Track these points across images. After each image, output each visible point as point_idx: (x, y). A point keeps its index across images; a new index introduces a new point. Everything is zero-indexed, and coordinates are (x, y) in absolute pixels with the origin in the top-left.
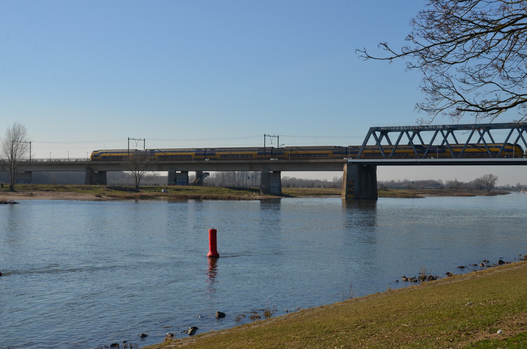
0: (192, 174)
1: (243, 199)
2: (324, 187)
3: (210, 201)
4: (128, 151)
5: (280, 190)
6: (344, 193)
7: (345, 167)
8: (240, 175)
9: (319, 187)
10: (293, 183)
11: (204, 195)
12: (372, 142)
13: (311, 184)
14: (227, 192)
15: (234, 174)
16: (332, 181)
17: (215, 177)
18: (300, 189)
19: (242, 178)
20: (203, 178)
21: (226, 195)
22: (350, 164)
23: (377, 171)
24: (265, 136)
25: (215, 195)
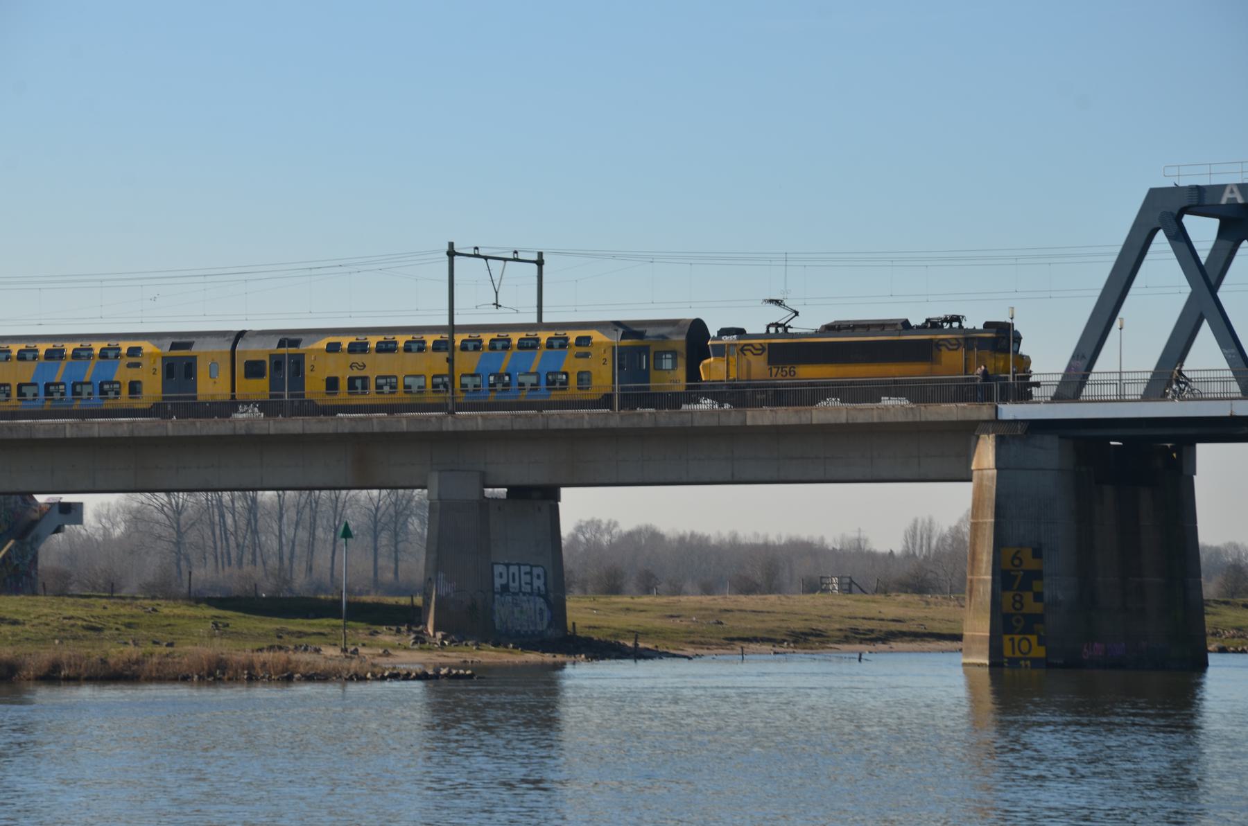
1: (309, 678)
2: (849, 587)
3: (86, 692)
4: (449, 340)
5: (558, 611)
6: (978, 626)
7: (985, 455)
8: (290, 515)
9: (814, 586)
10: (643, 566)
11: (46, 655)
12: (772, 330)
13: (763, 569)
14: (205, 628)
15: (253, 507)
16: (898, 548)
17: (118, 532)
18: (691, 600)
19: (303, 535)
20: (38, 539)
21: (200, 647)
22: (1012, 437)
23: (1197, 479)
24: (452, 253)
25: (118, 652)
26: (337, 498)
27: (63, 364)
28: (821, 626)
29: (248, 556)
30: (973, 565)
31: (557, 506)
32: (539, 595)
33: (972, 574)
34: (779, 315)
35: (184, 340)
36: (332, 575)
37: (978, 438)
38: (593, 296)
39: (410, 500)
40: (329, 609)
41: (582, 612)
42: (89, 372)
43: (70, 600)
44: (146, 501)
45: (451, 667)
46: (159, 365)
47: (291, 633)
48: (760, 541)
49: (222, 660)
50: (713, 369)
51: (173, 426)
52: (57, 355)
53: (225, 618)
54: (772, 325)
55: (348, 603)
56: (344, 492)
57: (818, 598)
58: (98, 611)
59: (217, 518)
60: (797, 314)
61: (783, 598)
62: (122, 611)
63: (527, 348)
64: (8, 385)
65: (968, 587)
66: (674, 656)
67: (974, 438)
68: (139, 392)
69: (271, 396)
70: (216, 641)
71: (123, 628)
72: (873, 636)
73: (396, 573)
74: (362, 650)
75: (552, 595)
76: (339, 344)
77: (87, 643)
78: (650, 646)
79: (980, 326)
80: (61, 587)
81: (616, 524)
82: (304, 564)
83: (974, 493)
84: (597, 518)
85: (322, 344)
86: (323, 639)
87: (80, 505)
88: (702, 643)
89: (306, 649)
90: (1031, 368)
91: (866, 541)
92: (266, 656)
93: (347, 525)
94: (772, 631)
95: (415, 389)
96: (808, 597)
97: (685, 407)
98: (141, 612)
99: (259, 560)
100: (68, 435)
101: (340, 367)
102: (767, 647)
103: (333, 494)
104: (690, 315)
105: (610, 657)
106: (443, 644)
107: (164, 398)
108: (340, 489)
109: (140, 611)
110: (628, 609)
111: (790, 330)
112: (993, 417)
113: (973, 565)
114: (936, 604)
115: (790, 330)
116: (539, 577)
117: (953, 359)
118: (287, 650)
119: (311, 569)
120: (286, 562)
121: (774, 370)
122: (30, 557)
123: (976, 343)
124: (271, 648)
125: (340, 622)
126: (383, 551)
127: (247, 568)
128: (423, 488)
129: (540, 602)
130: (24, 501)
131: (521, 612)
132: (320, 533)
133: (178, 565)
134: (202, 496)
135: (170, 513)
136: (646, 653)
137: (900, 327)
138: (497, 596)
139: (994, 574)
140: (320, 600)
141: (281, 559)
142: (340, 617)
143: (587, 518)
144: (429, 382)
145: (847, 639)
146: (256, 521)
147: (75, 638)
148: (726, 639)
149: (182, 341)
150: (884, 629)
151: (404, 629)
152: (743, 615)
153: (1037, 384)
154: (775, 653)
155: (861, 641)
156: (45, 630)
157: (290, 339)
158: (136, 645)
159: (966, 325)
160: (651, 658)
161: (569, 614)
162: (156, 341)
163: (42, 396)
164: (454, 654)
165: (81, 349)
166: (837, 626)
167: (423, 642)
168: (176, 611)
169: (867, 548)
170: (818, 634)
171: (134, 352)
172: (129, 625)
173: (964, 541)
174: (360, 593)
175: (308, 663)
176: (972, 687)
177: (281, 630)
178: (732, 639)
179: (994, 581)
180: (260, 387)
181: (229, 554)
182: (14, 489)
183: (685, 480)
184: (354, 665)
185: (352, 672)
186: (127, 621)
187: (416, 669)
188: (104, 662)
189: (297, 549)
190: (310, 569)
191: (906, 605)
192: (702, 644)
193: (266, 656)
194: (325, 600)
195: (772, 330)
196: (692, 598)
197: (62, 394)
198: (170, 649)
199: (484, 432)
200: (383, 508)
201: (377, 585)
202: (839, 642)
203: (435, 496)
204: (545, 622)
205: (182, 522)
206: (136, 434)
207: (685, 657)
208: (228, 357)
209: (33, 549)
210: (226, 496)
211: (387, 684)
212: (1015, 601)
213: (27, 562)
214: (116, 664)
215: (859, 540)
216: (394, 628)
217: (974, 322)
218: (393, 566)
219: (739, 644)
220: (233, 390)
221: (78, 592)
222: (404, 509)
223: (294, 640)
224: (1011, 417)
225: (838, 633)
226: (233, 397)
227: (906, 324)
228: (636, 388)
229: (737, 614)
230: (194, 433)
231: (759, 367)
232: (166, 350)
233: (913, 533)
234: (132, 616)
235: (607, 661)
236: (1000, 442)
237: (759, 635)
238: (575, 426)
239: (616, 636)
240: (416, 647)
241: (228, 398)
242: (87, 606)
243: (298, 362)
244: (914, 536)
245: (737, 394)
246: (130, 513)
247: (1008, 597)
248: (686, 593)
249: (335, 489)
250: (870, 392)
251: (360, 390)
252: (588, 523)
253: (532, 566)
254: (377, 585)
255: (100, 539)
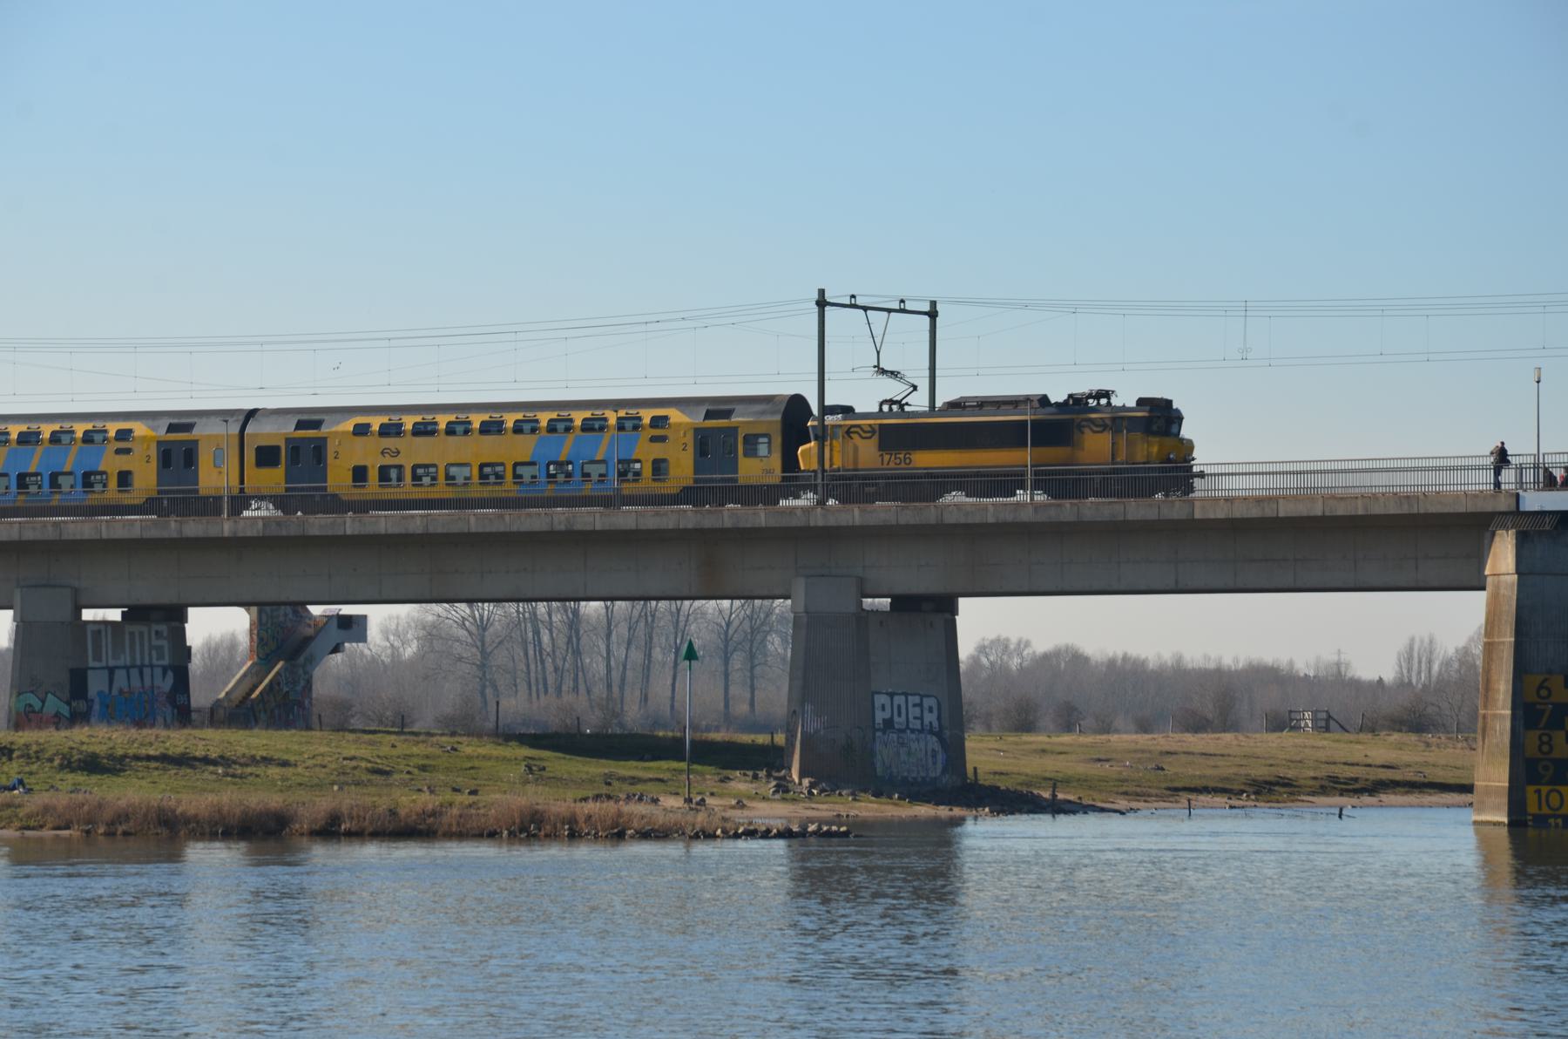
0: (217, 628)
1: (645, 835)
2: (1326, 724)
3: (370, 851)
5: (955, 752)
6: (1494, 774)
7: (1503, 556)
8: (622, 630)
9: (1281, 722)
10: (1063, 696)
11: (322, 804)
12: (886, 408)
13: (1217, 700)
15: (575, 622)
16: (1389, 674)
17: (410, 651)
19: (637, 656)
20: (312, 661)
21: (509, 794)
24: (822, 303)
25: (411, 802)
26: (678, 610)
27: (39, 450)
28: (1290, 774)
29: (568, 684)
30: (1486, 697)
31: (954, 621)
32: (931, 732)
33: (1485, 707)
34: (893, 389)
35: (184, 421)
36: (672, 707)
37: (1493, 534)
38: (998, 361)
39: (769, 614)
40: (668, 749)
41: (985, 754)
42: (70, 460)
43: (351, 736)
44: (444, 614)
45: (821, 822)
46: (153, 452)
47: (622, 779)
48: (1212, 666)
49: (537, 812)
50: (807, 453)
51: (174, 527)
52: (33, 439)
53: (541, 759)
54: (885, 402)
55: (692, 742)
56: (687, 603)
57: (1286, 738)
58: (385, 750)
59: (530, 635)
60: (915, 388)
61: (1241, 737)
62: (415, 750)
63: (592, 429)
64: (435, 466)
65: (1480, 724)
66: (1103, 810)
67: (1488, 535)
68: (667, 474)
69: (696, 481)
70: (530, 788)
71: (416, 771)
72: (1357, 786)
73: (752, 704)
74: (709, 801)
75: (947, 733)
76: (368, 425)
77: (372, 790)
78: (1071, 797)
79: (1132, 404)
80: (340, 720)
81: (1027, 644)
82: (638, 693)
83: (1488, 605)
84: (1004, 636)
85: (348, 425)
86: (662, 786)
87: (363, 619)
88: (1137, 795)
89: (640, 799)
90: (1195, 455)
91: (1348, 665)
92: (591, 807)
93: (691, 644)
94: (1227, 779)
95: (460, 481)
96: (1273, 736)
97: (782, 503)
98: (438, 751)
99: (582, 687)
100: (349, 532)
101: (369, 454)
102: (1220, 800)
103: (674, 605)
104: (789, 390)
105: (1021, 812)
106: (810, 793)
107: (159, 492)
108: (683, 598)
109: (437, 751)
110: (1044, 751)
111: (907, 408)
112: (1513, 508)
113: (1486, 697)
114: (1438, 746)
115: (907, 408)
116: (931, 710)
117: (1096, 447)
118: (617, 801)
119: (646, 699)
120: (615, 689)
121: (887, 457)
122: (302, 683)
123: (1125, 423)
124: (597, 797)
125: (683, 765)
126: (736, 676)
127: (568, 698)
128: (786, 597)
129: (933, 742)
130: (295, 612)
131: (909, 754)
132: (657, 654)
133: (483, 694)
134: (511, 608)
135: (473, 629)
136: (1067, 807)
137: (1036, 404)
138: (878, 734)
139: (1514, 708)
140: (657, 737)
141: (609, 686)
142: (683, 759)
143: (992, 636)
144: (476, 472)
145: (1323, 790)
146: (578, 640)
147: (357, 784)
148: (1169, 789)
149: (181, 422)
150: (1372, 777)
151: (763, 774)
152: (1191, 758)
153: (1202, 475)
154: (1231, 807)
155: (1342, 793)
156: (321, 773)
157: (309, 420)
158: (432, 792)
159: (1115, 402)
160: (1074, 812)
161: (969, 756)
162: (150, 422)
163: (14, 488)
164: (824, 807)
165: (594, 419)
166: (1312, 774)
167: (787, 791)
168: (482, 751)
169: (1349, 675)
170: (1286, 783)
171: (123, 435)
172: (423, 768)
173: (1474, 666)
174: (708, 729)
175: (643, 817)
176: (1485, 845)
177: (610, 775)
178: (1177, 790)
179: (1514, 717)
180: (274, 478)
181: (545, 679)
182: (283, 598)
183: (1115, 588)
184: (701, 818)
185: (698, 828)
186: (421, 762)
187: (778, 825)
188: (393, 813)
189: (629, 674)
190: (645, 699)
191: (1400, 747)
192: (1137, 796)
193: (591, 807)
194: (665, 738)
195: (886, 408)
196: (1125, 737)
197: (434, 479)
198: (473, 798)
199: (862, 527)
200: (735, 624)
201: (728, 719)
202: (1313, 794)
203: (801, 609)
204: (939, 766)
205: (488, 639)
206: (431, 530)
207: (1115, 811)
208: (236, 441)
209: (306, 673)
210: (542, 607)
211: (741, 844)
212: (1542, 743)
213: (299, 688)
214: (408, 816)
215: (1338, 664)
216: (750, 773)
217: (1125, 398)
218: (748, 695)
219: (1184, 796)
220: (242, 482)
221: (361, 727)
222: (762, 624)
223: (627, 788)
224: (1536, 508)
225: (1311, 783)
226: (242, 490)
227: (1044, 400)
228: (723, 480)
229: (1183, 758)
230: (502, 529)
231: (868, 454)
232: (162, 433)
233: (1408, 656)
234: (427, 757)
235: (1017, 816)
236: (1523, 540)
237: (1211, 784)
238: (977, 519)
239: (1028, 784)
240: (777, 796)
241: (236, 492)
242: (371, 743)
243: (319, 449)
244: (1410, 659)
245: (850, 486)
246: (424, 628)
247: (1532, 738)
248: (1117, 731)
249: (676, 599)
250: (1004, 483)
251: (394, 482)
252: (992, 642)
253: (922, 697)
254: (728, 719)
255: (387, 660)
